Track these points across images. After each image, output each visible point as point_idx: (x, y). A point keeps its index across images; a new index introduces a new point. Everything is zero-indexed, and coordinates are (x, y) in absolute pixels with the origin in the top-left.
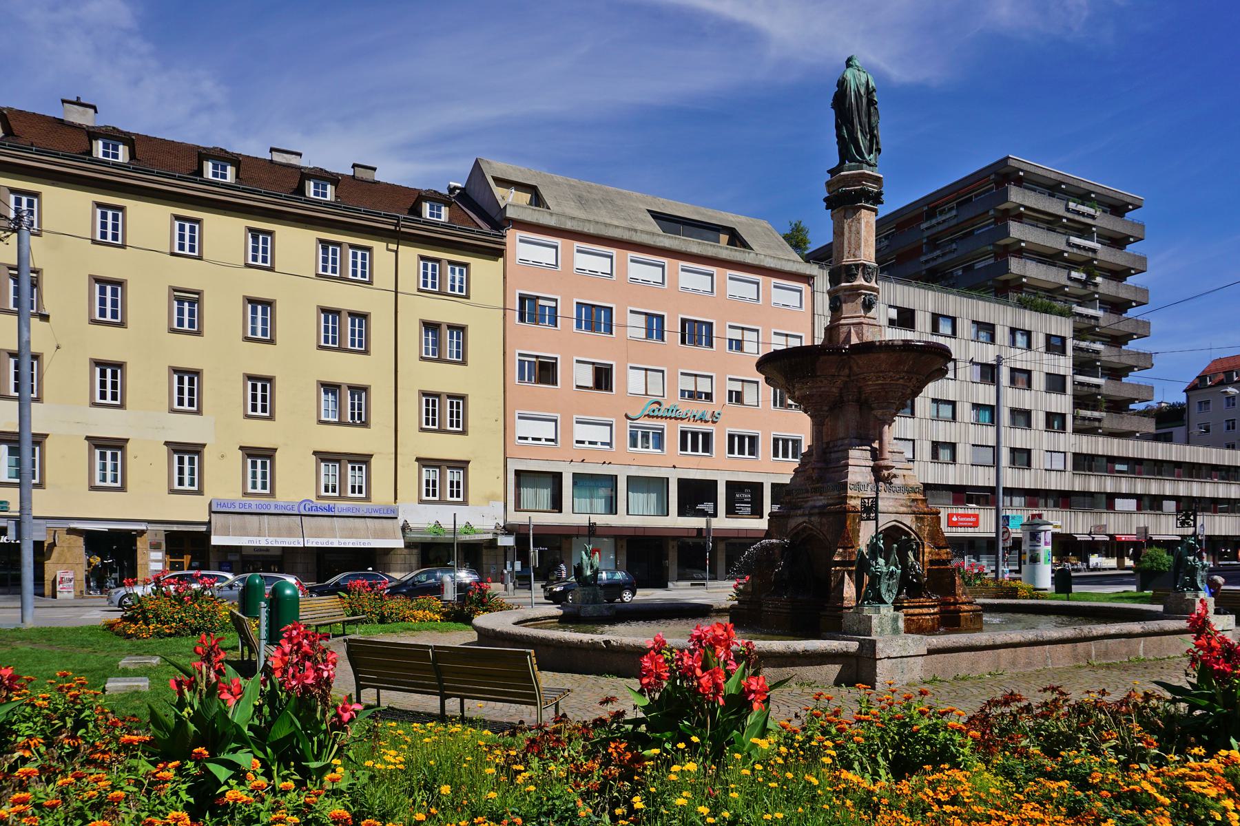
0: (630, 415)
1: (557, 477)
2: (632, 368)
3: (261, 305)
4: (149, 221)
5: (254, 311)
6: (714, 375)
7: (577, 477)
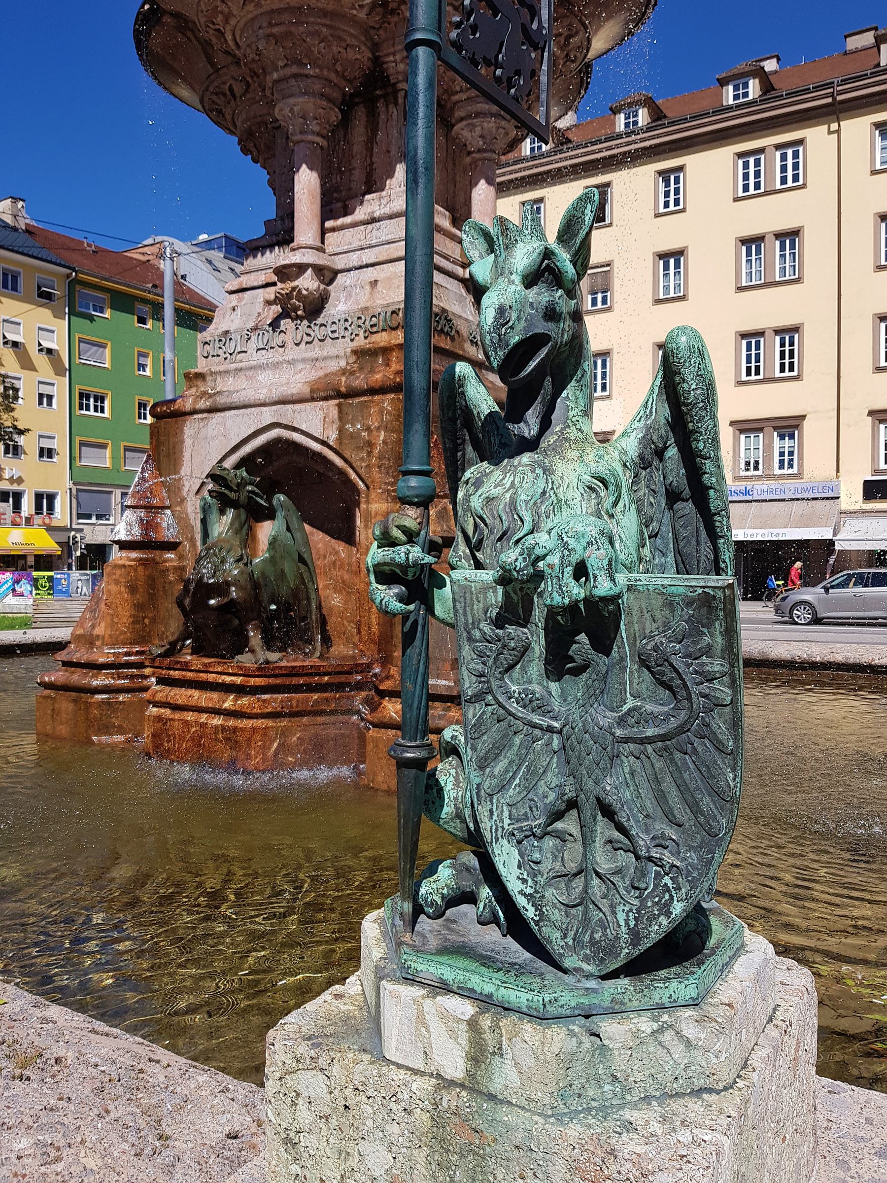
5: (666, 267)
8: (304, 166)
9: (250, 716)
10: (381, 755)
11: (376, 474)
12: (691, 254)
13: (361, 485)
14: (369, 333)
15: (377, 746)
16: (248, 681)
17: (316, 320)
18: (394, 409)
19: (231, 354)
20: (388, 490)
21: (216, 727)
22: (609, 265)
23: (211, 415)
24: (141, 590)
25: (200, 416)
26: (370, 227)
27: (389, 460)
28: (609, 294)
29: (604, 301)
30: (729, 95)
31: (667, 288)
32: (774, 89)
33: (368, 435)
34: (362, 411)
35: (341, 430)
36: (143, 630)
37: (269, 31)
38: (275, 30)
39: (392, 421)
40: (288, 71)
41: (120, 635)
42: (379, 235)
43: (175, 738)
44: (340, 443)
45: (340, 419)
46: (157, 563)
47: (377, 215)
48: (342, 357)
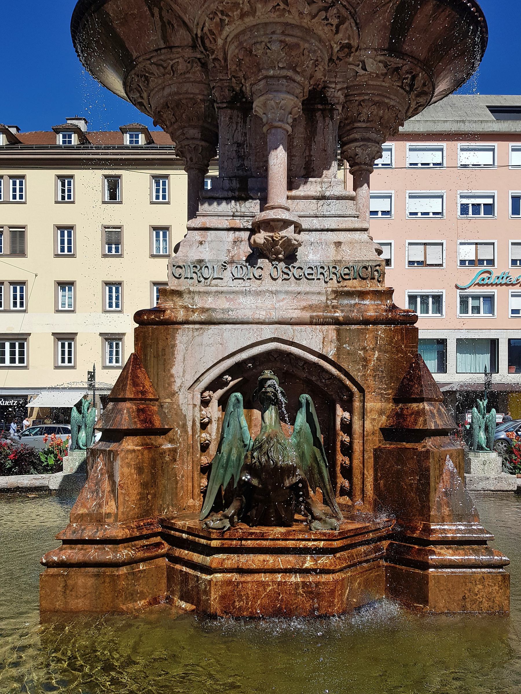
0: (460, 285)
1: (442, 342)
2: (461, 244)
3: (66, 230)
4: (89, 182)
5: (158, 236)
6: (444, 242)
8: (281, 147)
9: (333, 572)
10: (442, 588)
11: (371, 382)
13: (354, 389)
14: (343, 278)
15: (438, 582)
16: (331, 545)
17: (293, 263)
19: (206, 279)
20: (381, 394)
21: (297, 584)
22: (119, 228)
23: (204, 326)
24: (146, 471)
25: (191, 326)
26: (321, 202)
27: (382, 372)
28: (120, 246)
29: (117, 250)
30: (127, 139)
31: (158, 248)
32: (154, 143)
33: (364, 353)
34: (358, 335)
35: (338, 349)
36: (147, 505)
37: (283, 38)
38: (288, 39)
40: (284, 73)
41: (130, 511)
42: (329, 209)
43: (247, 598)
44: (339, 358)
45: (338, 340)
46: (156, 447)
47: (327, 194)
48: (322, 294)
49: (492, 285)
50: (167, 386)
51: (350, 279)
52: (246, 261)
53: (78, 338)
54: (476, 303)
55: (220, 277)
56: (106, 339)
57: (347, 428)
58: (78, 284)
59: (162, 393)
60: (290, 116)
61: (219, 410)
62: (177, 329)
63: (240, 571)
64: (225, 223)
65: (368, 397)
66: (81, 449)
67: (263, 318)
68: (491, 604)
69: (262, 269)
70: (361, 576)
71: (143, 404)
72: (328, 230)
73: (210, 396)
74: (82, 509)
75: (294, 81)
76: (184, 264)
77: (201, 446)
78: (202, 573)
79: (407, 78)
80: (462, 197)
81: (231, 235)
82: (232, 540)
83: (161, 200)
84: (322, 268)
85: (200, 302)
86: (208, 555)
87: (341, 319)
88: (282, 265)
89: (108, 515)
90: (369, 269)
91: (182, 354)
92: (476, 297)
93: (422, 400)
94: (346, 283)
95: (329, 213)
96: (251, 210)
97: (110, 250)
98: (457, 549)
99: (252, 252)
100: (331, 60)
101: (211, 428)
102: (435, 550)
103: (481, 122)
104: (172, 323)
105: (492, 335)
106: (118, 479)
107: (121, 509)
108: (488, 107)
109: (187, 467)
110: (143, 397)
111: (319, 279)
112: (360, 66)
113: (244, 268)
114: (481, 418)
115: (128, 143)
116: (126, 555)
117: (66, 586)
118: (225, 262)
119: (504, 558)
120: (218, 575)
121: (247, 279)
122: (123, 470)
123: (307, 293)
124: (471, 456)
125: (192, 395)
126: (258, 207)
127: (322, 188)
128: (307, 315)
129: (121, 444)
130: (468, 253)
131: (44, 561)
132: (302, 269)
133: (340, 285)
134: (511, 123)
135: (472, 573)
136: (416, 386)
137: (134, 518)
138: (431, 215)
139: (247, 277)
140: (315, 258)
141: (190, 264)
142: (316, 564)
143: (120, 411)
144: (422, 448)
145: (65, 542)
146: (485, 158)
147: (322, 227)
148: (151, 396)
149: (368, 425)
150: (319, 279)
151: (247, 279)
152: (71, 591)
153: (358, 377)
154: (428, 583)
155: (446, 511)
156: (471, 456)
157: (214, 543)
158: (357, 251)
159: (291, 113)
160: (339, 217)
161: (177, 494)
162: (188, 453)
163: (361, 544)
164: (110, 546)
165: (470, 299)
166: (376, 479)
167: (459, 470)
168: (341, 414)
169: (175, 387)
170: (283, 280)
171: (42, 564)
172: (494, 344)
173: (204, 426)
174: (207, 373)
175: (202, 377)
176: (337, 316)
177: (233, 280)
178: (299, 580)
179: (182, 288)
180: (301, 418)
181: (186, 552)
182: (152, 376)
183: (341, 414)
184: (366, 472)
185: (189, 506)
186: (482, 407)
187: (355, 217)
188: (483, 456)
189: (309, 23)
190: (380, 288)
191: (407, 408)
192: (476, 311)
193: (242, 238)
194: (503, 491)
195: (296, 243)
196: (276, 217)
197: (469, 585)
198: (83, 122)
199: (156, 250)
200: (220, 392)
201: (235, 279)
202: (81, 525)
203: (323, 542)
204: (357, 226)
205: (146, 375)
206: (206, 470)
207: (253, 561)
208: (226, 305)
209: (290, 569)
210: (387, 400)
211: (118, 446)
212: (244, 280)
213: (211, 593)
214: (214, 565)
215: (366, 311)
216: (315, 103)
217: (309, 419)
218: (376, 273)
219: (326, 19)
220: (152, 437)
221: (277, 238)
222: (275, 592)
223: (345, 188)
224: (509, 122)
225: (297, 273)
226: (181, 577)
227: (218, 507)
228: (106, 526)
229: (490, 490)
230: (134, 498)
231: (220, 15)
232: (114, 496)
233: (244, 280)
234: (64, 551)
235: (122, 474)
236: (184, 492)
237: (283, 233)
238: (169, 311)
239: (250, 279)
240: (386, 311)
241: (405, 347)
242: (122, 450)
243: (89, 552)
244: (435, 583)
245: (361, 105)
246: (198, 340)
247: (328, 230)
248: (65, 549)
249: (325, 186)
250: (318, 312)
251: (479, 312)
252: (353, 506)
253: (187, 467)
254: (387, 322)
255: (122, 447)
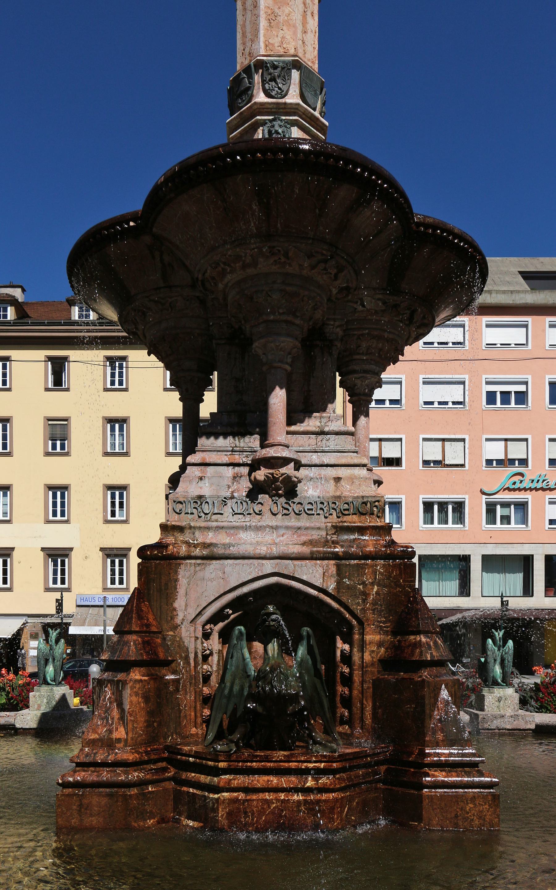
1: (466, 559)
2: (487, 440)
5: (113, 429)
6: (529, 437)
7: (485, 558)
10: (435, 807)
11: (370, 615)
12: (132, 422)
13: (354, 622)
14: (342, 513)
17: (293, 499)
18: (385, 571)
19: (206, 514)
21: (299, 801)
22: (66, 420)
23: (208, 562)
25: (193, 561)
26: (320, 437)
27: (381, 605)
28: (66, 442)
29: (63, 447)
31: (113, 445)
33: (363, 588)
35: (339, 583)
38: (289, 289)
39: (384, 580)
40: (284, 317)
41: (138, 737)
42: (328, 444)
47: (326, 429)
49: (525, 489)
50: (169, 619)
51: (349, 515)
52: (247, 496)
53: (15, 554)
54: (506, 512)
55: (220, 512)
56: (50, 556)
57: (347, 659)
58: (15, 489)
59: (165, 626)
60: (289, 356)
61: (219, 643)
62: (180, 564)
63: (246, 790)
64: (225, 459)
65: (367, 630)
66: (49, 684)
67: (264, 554)
68: (481, 821)
69: (262, 504)
70: (359, 797)
71: (147, 636)
72: (327, 466)
73: (211, 629)
74: (93, 735)
75: (294, 324)
76: (185, 500)
77: (203, 677)
78: (209, 793)
79: (406, 314)
80: (488, 383)
81: (229, 472)
82: (239, 762)
83: (117, 386)
84: (322, 503)
85: (200, 538)
86: (217, 775)
87: (341, 554)
88: (283, 500)
89: (119, 740)
90: (369, 504)
91: (185, 588)
92: (505, 505)
93: (419, 633)
94: (346, 518)
95: (328, 448)
96: (251, 445)
97: (54, 447)
98: (450, 771)
99: (251, 487)
100: (329, 300)
101: (212, 660)
102: (430, 772)
103: (512, 292)
104: (175, 559)
105: (525, 550)
106: (127, 707)
107: (130, 735)
108: (520, 272)
109: (190, 697)
110: (148, 630)
111: (319, 514)
112: (359, 303)
113: (244, 503)
114: (496, 651)
115: (77, 318)
116: (137, 776)
117: (81, 806)
118: (225, 498)
119: (494, 780)
120: (225, 794)
121: (248, 514)
122: (130, 698)
123: (307, 528)
124: (485, 691)
125: (193, 628)
126: (258, 443)
127: (321, 422)
128: (306, 550)
129: (129, 674)
130: (496, 451)
131: (60, 781)
132: (302, 504)
133: (339, 520)
134: (549, 294)
135: (464, 793)
136: (414, 619)
137: (142, 744)
138: (450, 405)
139: (247, 512)
140: (314, 493)
141: (190, 499)
142: (317, 784)
143: (127, 643)
144: (418, 678)
145: (78, 765)
146: (515, 336)
147: (321, 463)
148: (154, 629)
149: (367, 657)
150: (319, 514)
151: (248, 514)
152: (86, 809)
153: (358, 609)
154: (422, 802)
155: (440, 736)
156: (485, 691)
157: (222, 765)
158: (357, 486)
159: (290, 354)
160: (338, 452)
161: (180, 722)
162: (190, 684)
163: (359, 767)
164: (121, 769)
165: (498, 507)
166: (374, 708)
167: (455, 700)
168: (341, 646)
169: (178, 620)
170: (283, 515)
171: (58, 784)
172: (526, 562)
173: (205, 658)
174: (210, 607)
175: (204, 611)
176: (337, 552)
177: (233, 515)
178: (301, 798)
179: (183, 524)
180: (302, 651)
181: (193, 775)
182: (155, 609)
183: (341, 646)
184: (365, 702)
185: (192, 734)
186: (498, 638)
187: (354, 452)
188: (498, 692)
189: (309, 273)
190: (379, 524)
191: (405, 641)
192: (505, 521)
193: (241, 473)
194: (520, 730)
195: (296, 480)
196: (276, 455)
197: (461, 804)
198: (19, 290)
199: (111, 447)
200: (221, 625)
201: (236, 514)
202: (93, 750)
203: (323, 764)
204: (356, 461)
205: (150, 609)
206: (206, 700)
207: (258, 781)
208: (227, 540)
209: (292, 788)
210: (386, 633)
211: (126, 676)
212: (244, 515)
213: (219, 810)
214: (222, 784)
215: (365, 547)
216: (314, 341)
217: (310, 650)
218: (375, 509)
219: (325, 269)
220: (157, 668)
221: (277, 475)
222: (279, 809)
223: (345, 423)
224: (546, 292)
225: (297, 508)
226: (188, 797)
227: (219, 737)
228: (117, 751)
229: (505, 729)
230: (141, 725)
231: (222, 265)
232: (124, 723)
233: (244, 515)
234: (78, 773)
235: (131, 702)
236: (187, 721)
237: (283, 470)
238: (171, 547)
239: (250, 514)
240: (385, 546)
241: (403, 581)
242: (131, 680)
243: (102, 773)
244: (429, 802)
245: (360, 339)
246: (200, 574)
247: (327, 466)
248: (79, 771)
249: (324, 420)
250: (318, 547)
251: (509, 523)
252: (352, 734)
253: (190, 697)
254: (385, 557)
255: (130, 677)
